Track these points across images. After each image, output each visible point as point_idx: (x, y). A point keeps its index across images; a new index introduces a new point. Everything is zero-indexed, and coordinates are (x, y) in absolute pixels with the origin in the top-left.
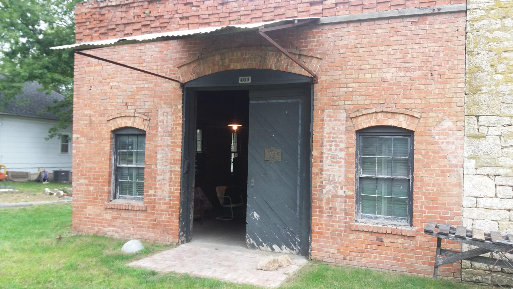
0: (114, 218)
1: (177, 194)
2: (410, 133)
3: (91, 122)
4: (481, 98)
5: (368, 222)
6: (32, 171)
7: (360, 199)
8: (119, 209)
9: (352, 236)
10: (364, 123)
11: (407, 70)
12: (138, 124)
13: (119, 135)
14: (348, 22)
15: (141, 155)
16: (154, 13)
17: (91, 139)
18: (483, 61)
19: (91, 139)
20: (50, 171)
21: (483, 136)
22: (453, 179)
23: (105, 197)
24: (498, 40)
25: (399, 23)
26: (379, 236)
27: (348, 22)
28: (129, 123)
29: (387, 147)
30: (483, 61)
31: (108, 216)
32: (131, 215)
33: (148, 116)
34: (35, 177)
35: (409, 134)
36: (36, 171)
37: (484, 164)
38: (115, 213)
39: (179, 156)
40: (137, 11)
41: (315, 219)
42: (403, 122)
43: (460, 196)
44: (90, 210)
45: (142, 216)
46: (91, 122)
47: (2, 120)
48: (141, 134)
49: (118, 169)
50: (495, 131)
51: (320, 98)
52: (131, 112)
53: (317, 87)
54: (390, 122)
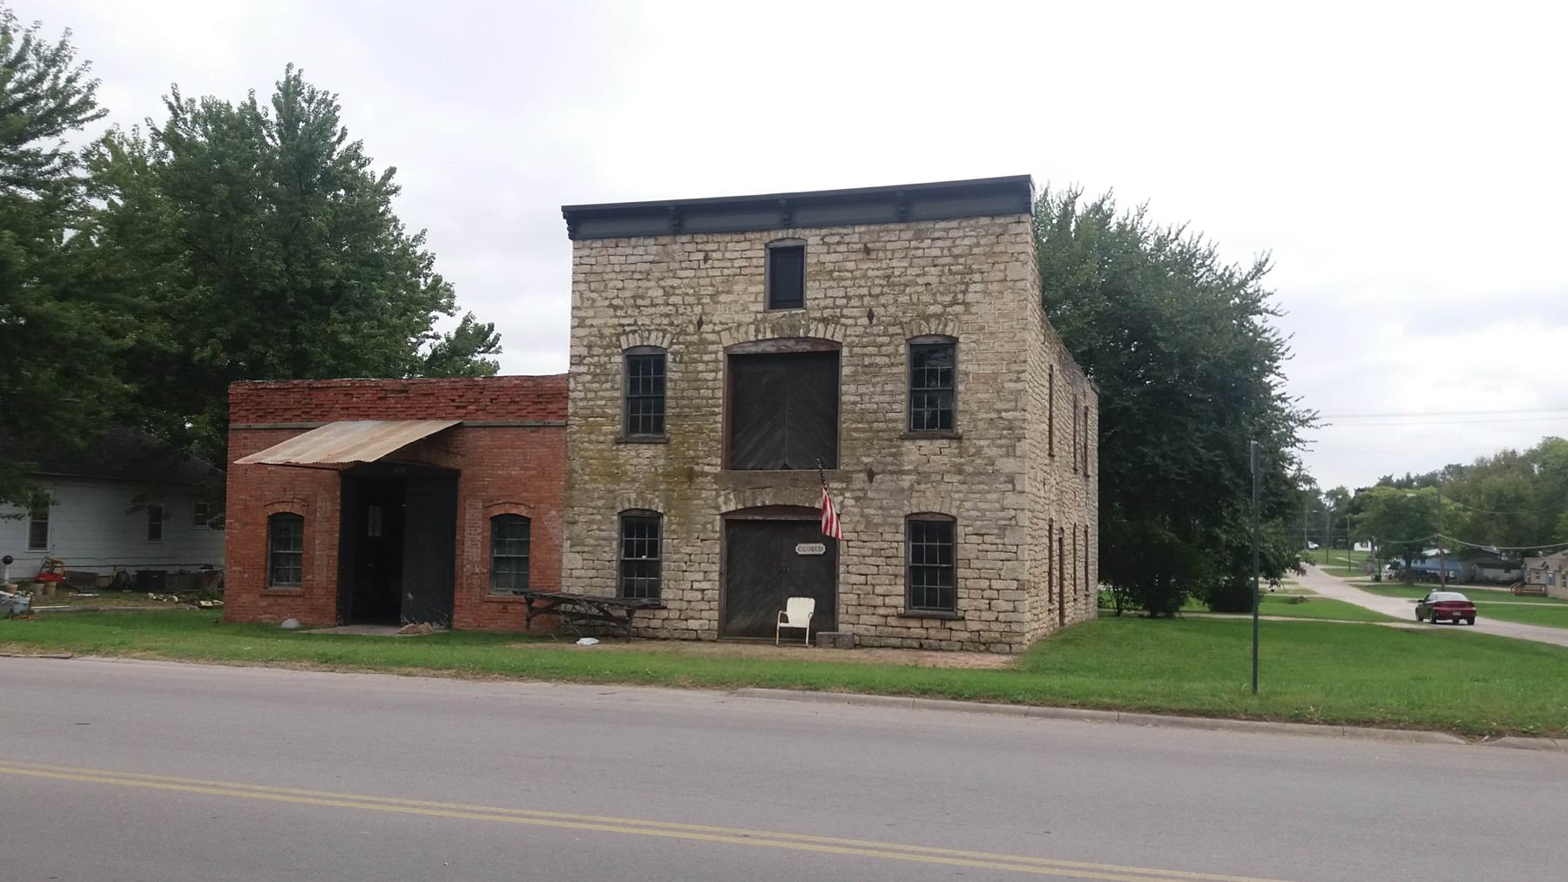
0: (270, 605)
1: (334, 578)
2: (528, 520)
3: (246, 507)
4: (575, 493)
5: (497, 595)
6: (102, 572)
7: (494, 575)
8: (276, 596)
9: (485, 607)
10: (496, 512)
11: (527, 469)
12: (297, 509)
13: (275, 520)
14: (485, 427)
15: (299, 543)
16: (315, 401)
17: (247, 524)
18: (576, 465)
19: (247, 524)
20: (132, 572)
21: (575, 523)
22: (556, 556)
23: (261, 584)
24: (585, 450)
25: (522, 431)
26: (783, 236)
27: (485, 427)
28: (280, 508)
29: (511, 532)
30: (576, 465)
31: (264, 603)
32: (288, 600)
33: (307, 502)
34: (105, 582)
35: (527, 521)
36: (110, 572)
37: (576, 542)
38: (271, 600)
39: (336, 542)
40: (297, 396)
41: (457, 595)
42: (522, 511)
43: (560, 569)
44: (244, 598)
45: (299, 601)
46: (246, 507)
47: (1551, 450)
48: (299, 519)
49: (275, 558)
50: (583, 519)
51: (464, 489)
52: (289, 497)
53: (461, 479)
54: (514, 511)
